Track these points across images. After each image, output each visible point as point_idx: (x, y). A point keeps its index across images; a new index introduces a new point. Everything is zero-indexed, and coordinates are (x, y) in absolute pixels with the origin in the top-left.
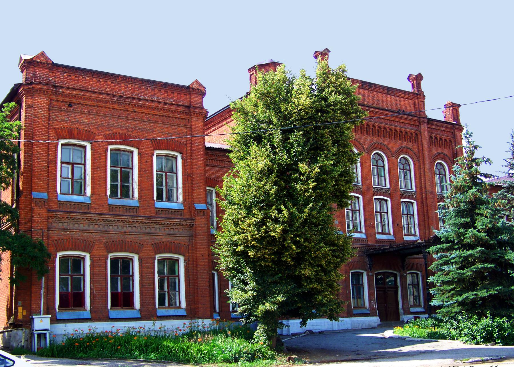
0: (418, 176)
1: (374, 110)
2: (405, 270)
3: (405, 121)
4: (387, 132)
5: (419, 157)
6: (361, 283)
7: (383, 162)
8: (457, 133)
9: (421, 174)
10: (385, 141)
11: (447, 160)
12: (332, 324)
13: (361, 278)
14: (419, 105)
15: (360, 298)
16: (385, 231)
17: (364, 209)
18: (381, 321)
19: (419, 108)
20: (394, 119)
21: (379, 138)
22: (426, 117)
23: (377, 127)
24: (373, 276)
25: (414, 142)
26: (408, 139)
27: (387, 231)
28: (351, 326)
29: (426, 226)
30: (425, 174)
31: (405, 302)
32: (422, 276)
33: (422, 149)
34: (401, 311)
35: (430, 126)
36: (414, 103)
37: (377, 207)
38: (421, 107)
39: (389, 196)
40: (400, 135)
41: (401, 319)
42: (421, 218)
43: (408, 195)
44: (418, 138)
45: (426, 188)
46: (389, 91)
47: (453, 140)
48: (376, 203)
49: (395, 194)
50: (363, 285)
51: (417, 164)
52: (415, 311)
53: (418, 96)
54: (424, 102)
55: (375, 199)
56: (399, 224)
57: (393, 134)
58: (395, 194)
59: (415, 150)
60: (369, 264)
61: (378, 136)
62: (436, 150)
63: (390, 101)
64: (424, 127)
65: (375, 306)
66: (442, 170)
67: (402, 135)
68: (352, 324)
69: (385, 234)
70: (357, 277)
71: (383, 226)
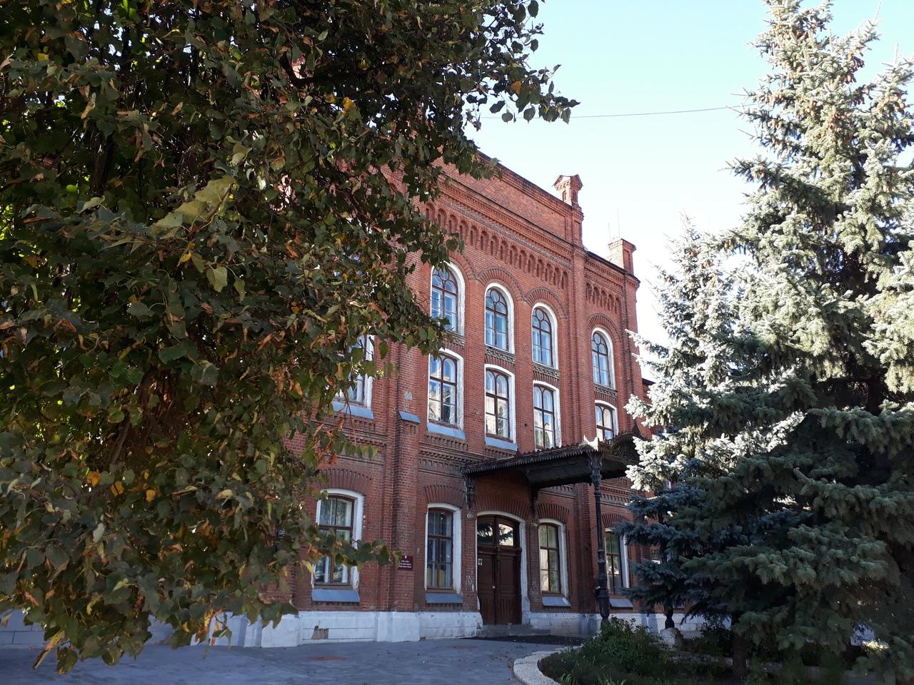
0: (564, 345)
1: (498, 208)
2: (537, 517)
3: (548, 246)
4: (516, 255)
5: (568, 312)
6: (448, 534)
7: (506, 307)
8: (628, 288)
9: (569, 342)
10: (513, 270)
11: (612, 330)
12: (377, 622)
13: (448, 523)
14: (572, 226)
15: (443, 568)
16: (498, 424)
17: (465, 382)
18: (484, 623)
19: (572, 231)
20: (530, 236)
21: (503, 262)
22: (583, 249)
23: (500, 240)
24: (474, 519)
25: (560, 285)
26: (605, 302)
27: (505, 435)
28: (420, 632)
29: (576, 436)
30: (576, 342)
31: (534, 583)
32: (567, 532)
33: (575, 301)
34: (525, 605)
35: (588, 267)
36: (565, 222)
37: (489, 385)
38: (576, 231)
39: (514, 368)
40: (538, 267)
41: (524, 621)
42: (568, 418)
43: (545, 374)
44: (567, 281)
45: (577, 367)
46: (526, 186)
47: (622, 300)
48: (488, 379)
49: (529, 375)
50: (451, 539)
51: (564, 324)
52: (553, 604)
53: (572, 212)
54: (580, 224)
55: (488, 369)
56: (529, 424)
57: (527, 262)
58: (529, 375)
59: (562, 299)
60: (469, 495)
61: (502, 258)
62: (595, 309)
63: (524, 204)
64: (579, 264)
65: (474, 588)
66: (602, 347)
67: (543, 268)
68: (421, 628)
69: (503, 439)
70: (442, 517)
71: (498, 424)
